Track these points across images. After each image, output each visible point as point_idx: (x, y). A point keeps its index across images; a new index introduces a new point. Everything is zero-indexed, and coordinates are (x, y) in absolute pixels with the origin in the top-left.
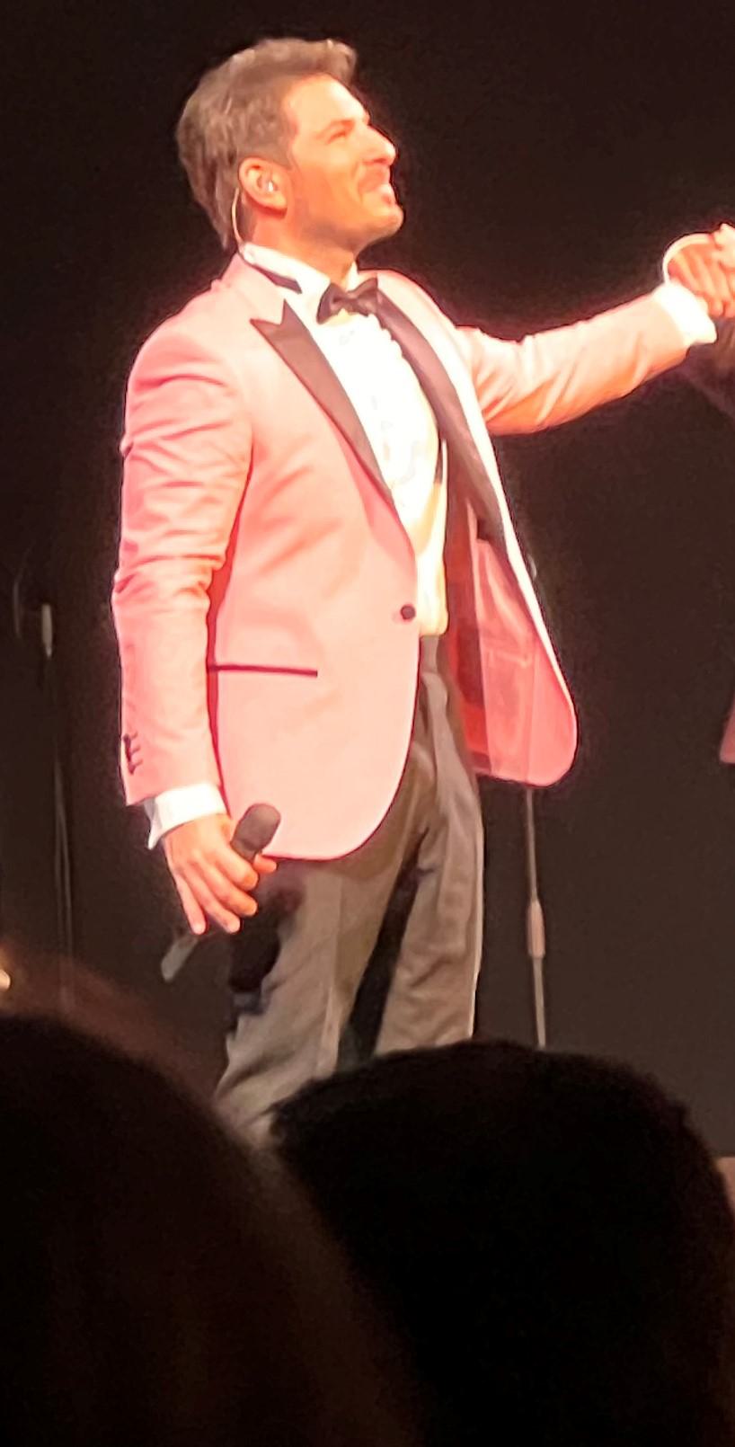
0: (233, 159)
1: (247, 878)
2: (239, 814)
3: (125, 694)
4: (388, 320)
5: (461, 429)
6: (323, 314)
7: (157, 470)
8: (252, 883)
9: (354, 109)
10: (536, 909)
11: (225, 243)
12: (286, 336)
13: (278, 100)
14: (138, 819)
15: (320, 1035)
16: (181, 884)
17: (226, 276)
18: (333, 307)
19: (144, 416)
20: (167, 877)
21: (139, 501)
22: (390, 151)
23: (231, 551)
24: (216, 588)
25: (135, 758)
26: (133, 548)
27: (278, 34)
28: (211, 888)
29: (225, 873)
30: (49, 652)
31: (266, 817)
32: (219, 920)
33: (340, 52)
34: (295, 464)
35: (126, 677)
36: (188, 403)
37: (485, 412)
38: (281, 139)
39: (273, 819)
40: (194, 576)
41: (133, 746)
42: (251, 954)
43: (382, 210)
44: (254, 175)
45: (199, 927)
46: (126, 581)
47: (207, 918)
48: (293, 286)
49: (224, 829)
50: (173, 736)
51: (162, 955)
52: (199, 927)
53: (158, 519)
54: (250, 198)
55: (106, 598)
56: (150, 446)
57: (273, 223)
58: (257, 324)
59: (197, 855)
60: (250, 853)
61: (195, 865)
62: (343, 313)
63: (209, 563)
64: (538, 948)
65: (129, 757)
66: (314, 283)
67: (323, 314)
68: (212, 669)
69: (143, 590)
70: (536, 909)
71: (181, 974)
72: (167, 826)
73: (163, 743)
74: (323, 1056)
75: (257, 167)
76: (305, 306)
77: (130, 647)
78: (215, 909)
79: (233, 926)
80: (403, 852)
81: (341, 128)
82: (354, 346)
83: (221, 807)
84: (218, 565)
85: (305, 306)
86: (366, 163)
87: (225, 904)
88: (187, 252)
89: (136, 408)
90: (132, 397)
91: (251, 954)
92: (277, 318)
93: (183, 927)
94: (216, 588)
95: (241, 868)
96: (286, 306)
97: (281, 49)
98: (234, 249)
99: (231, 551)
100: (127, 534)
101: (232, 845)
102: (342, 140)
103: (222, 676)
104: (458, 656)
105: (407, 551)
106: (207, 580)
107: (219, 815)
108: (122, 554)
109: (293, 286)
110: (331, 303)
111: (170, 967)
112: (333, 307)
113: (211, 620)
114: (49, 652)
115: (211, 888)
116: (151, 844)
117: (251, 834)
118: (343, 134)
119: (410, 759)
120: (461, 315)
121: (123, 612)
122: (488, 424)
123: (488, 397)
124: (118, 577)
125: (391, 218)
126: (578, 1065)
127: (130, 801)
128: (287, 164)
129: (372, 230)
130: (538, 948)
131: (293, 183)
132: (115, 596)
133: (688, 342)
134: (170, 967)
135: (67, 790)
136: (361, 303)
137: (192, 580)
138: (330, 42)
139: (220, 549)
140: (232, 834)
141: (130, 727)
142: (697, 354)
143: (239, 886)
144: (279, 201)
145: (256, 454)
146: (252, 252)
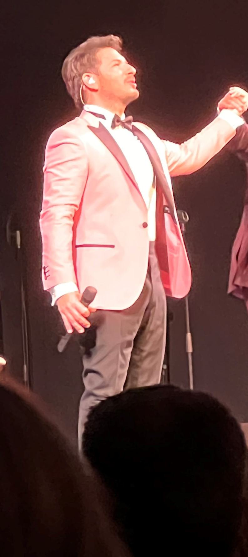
0: (81, 75)
1: (86, 312)
2: (82, 290)
3: (43, 253)
4: (136, 133)
5: (161, 171)
6: (113, 126)
7: (56, 175)
8: (87, 316)
9: (123, 59)
10: (189, 335)
11: (77, 106)
12: (100, 132)
13: (94, 54)
14: (47, 295)
15: (115, 379)
16: (63, 316)
17: (81, 116)
18: (117, 123)
19: (50, 157)
20: (58, 314)
21: (49, 186)
22: (134, 70)
23: (81, 204)
24: (76, 217)
25: (47, 274)
26: (47, 202)
27: (95, 35)
28: (73, 320)
29: (78, 311)
30: (19, 247)
31: (92, 291)
32: (76, 328)
33: (116, 39)
34: (103, 174)
35: (44, 247)
36: (66, 152)
37: (169, 167)
38: (96, 66)
39: (94, 291)
40: (68, 211)
41: (46, 271)
42: (88, 341)
43: (133, 92)
44: (86, 78)
45: (70, 331)
46: (44, 214)
47: (73, 328)
48: (103, 117)
49: (78, 296)
50: (61, 266)
51: (58, 342)
52: (70, 331)
53: (56, 192)
54: (86, 86)
55: (38, 221)
56: (53, 167)
57: (94, 94)
58: (90, 127)
59: (69, 305)
60: (86, 304)
61: (68, 309)
62: (120, 127)
63: (73, 207)
64: (190, 349)
65: (45, 273)
66: (110, 116)
67: (113, 126)
68: (75, 247)
69: (50, 217)
70: (189, 335)
71: (65, 350)
72: (57, 297)
73: (57, 268)
74: (117, 387)
75: (88, 76)
76: (107, 124)
77: (46, 237)
78: (76, 324)
79: (82, 331)
80: (144, 306)
81: (117, 63)
82: (122, 136)
83: (76, 289)
84: (77, 209)
85: (107, 124)
86: (126, 74)
87: (78, 322)
88: (65, 107)
89: (48, 157)
90: (47, 154)
91: (88, 341)
92: (97, 126)
93: (64, 332)
94: (76, 217)
95: (84, 310)
96: (100, 124)
97: (95, 40)
98: (82, 106)
99: (81, 204)
100: (45, 198)
101: (81, 302)
102: (117, 67)
103: (78, 249)
104: (160, 248)
105: (145, 210)
106: (73, 214)
107: (76, 292)
108: (43, 205)
109: (103, 117)
110: (116, 122)
111: (61, 348)
112: (117, 123)
113: (74, 229)
114: (19, 247)
115: (73, 320)
116: (53, 304)
117: (87, 297)
118: (118, 65)
119: (145, 284)
120: (162, 136)
121: (43, 224)
122: (170, 173)
123: (170, 163)
124: (42, 213)
125: (135, 93)
126: (205, 396)
127: (45, 289)
128: (98, 74)
129: (129, 98)
130: (190, 349)
131: (100, 80)
132: (41, 220)
133: (235, 128)
134: (61, 348)
135: (26, 296)
136: (126, 124)
137: (68, 213)
138: (112, 36)
139: (78, 203)
140: (80, 298)
141: (45, 263)
142: (239, 130)
143: (83, 315)
144: (96, 87)
145: (89, 172)
146: (87, 107)
